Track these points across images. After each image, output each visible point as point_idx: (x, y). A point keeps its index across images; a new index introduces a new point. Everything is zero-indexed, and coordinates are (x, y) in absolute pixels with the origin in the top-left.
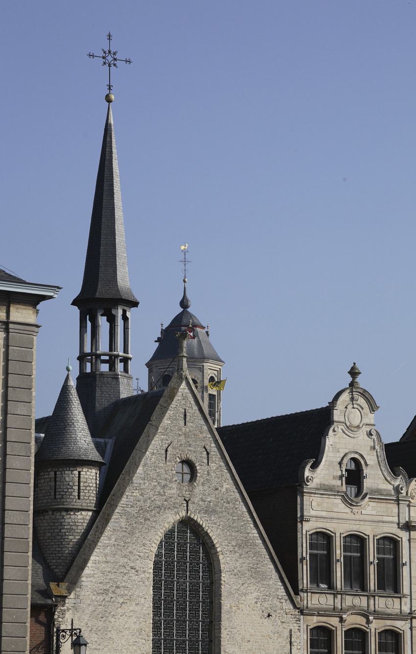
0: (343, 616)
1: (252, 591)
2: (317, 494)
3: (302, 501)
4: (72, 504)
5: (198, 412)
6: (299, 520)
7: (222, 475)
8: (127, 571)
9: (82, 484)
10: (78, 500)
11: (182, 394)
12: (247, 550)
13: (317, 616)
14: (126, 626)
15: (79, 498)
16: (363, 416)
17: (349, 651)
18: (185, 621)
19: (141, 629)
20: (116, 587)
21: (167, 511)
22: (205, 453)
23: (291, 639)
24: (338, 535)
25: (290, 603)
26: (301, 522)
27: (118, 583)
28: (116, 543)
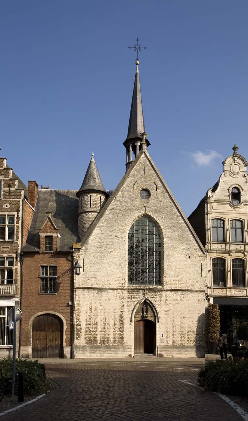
0: (231, 253)
1: (181, 246)
2: (216, 203)
3: (207, 206)
4: (88, 209)
5: (151, 168)
6: (206, 214)
7: (164, 195)
8: (113, 238)
9: (92, 201)
10: (90, 208)
11: (143, 160)
12: (177, 228)
13: (216, 253)
14: (113, 262)
15: (91, 207)
16: (240, 168)
17: (234, 269)
18: (146, 260)
19: (121, 263)
20: (107, 245)
21: (134, 211)
22: (155, 185)
23: (202, 268)
24: (227, 219)
25: (201, 252)
26: (207, 214)
27: (108, 243)
28: (107, 225)
